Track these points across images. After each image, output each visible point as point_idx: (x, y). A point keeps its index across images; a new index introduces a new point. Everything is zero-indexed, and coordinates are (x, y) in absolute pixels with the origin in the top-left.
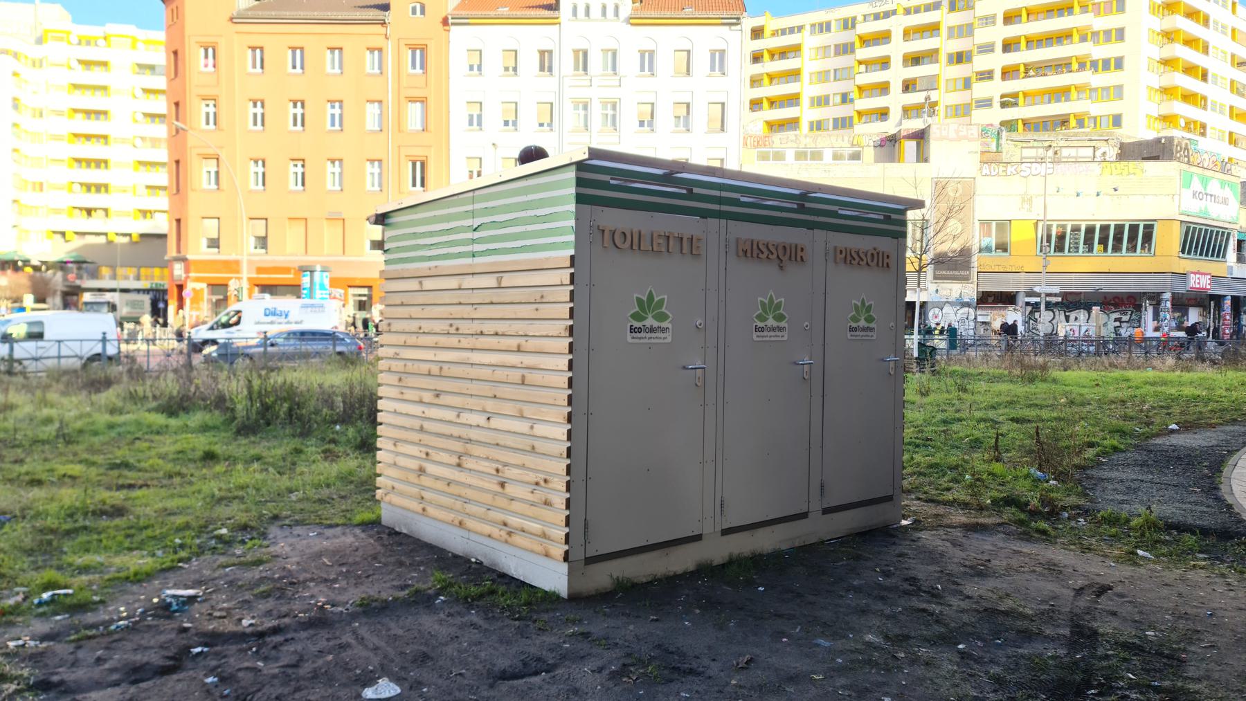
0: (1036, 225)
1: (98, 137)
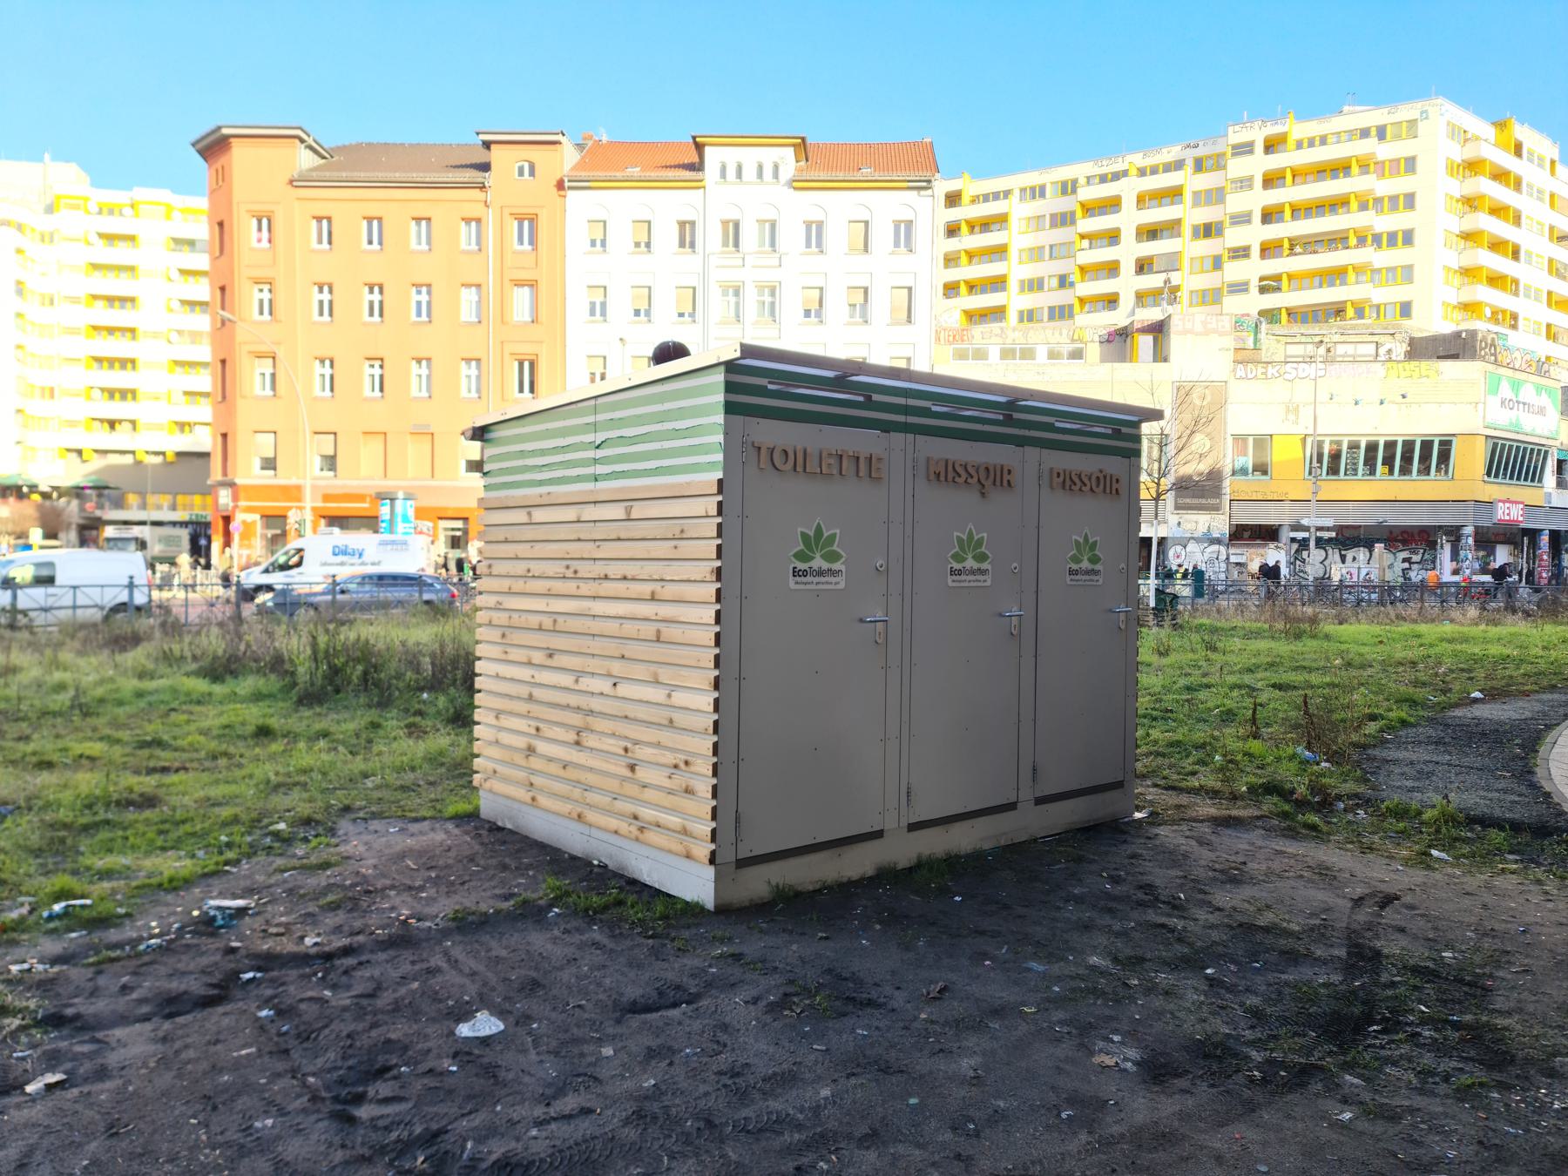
0: (1304, 440)
1: (123, 330)
